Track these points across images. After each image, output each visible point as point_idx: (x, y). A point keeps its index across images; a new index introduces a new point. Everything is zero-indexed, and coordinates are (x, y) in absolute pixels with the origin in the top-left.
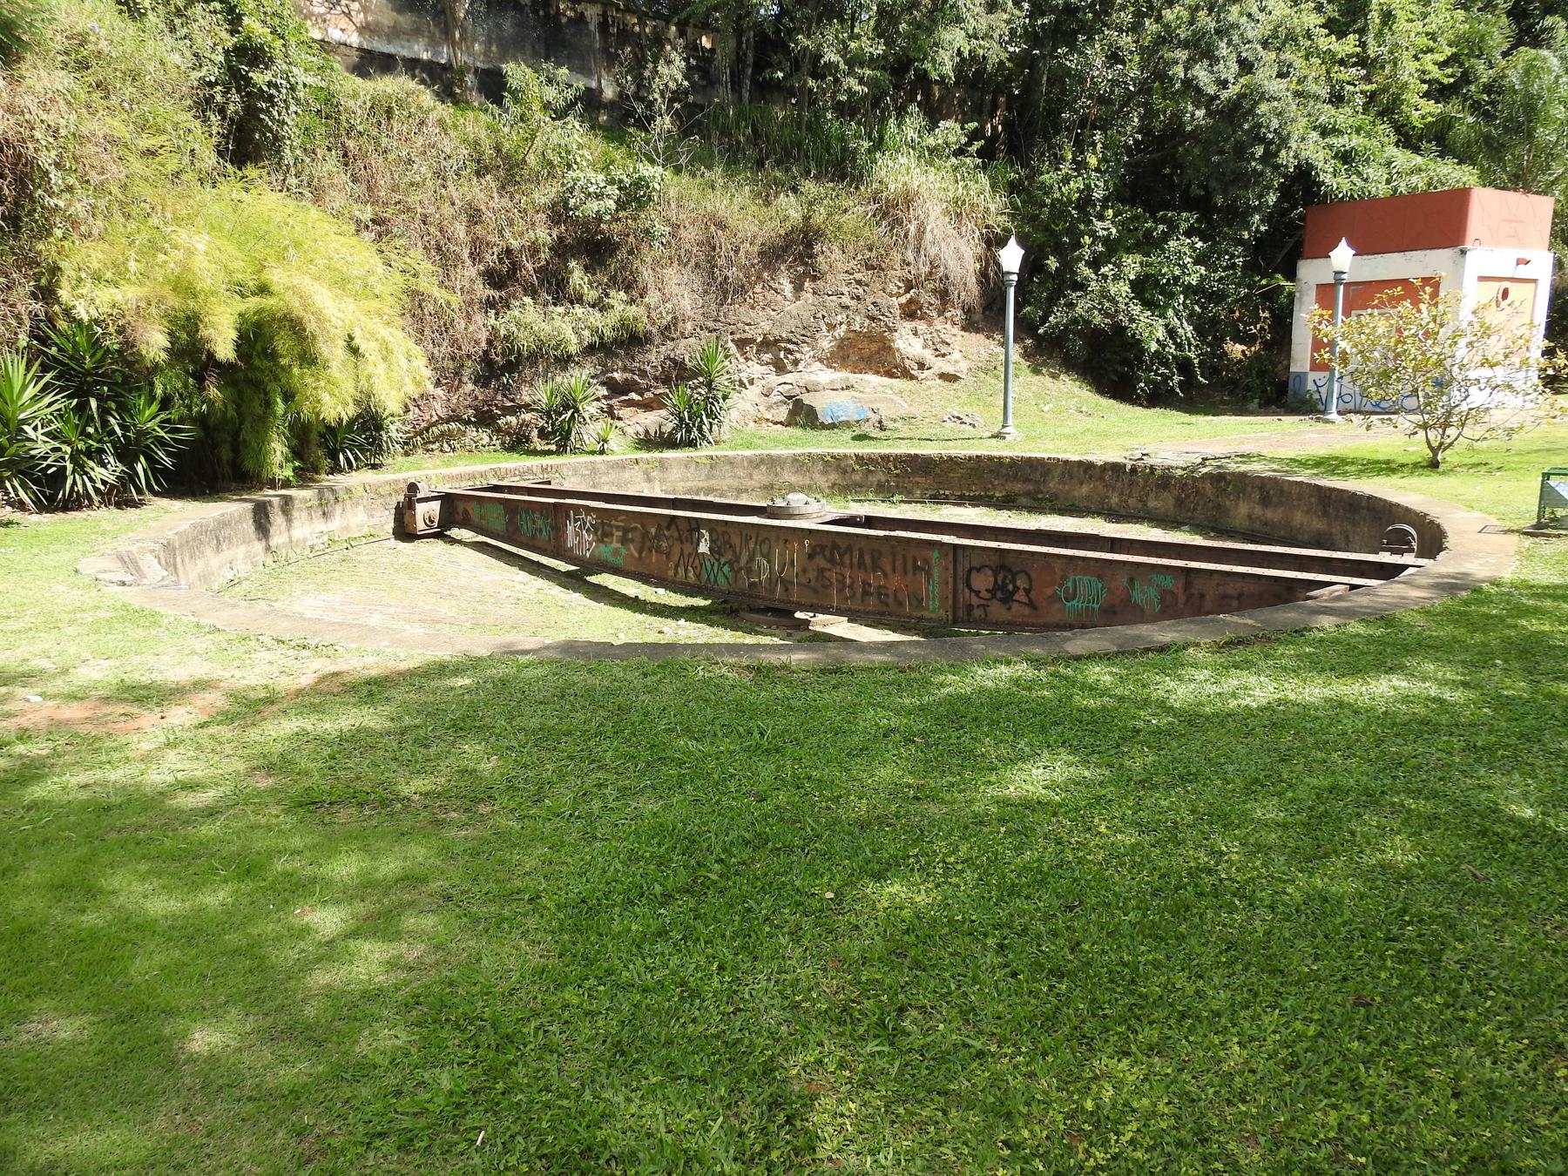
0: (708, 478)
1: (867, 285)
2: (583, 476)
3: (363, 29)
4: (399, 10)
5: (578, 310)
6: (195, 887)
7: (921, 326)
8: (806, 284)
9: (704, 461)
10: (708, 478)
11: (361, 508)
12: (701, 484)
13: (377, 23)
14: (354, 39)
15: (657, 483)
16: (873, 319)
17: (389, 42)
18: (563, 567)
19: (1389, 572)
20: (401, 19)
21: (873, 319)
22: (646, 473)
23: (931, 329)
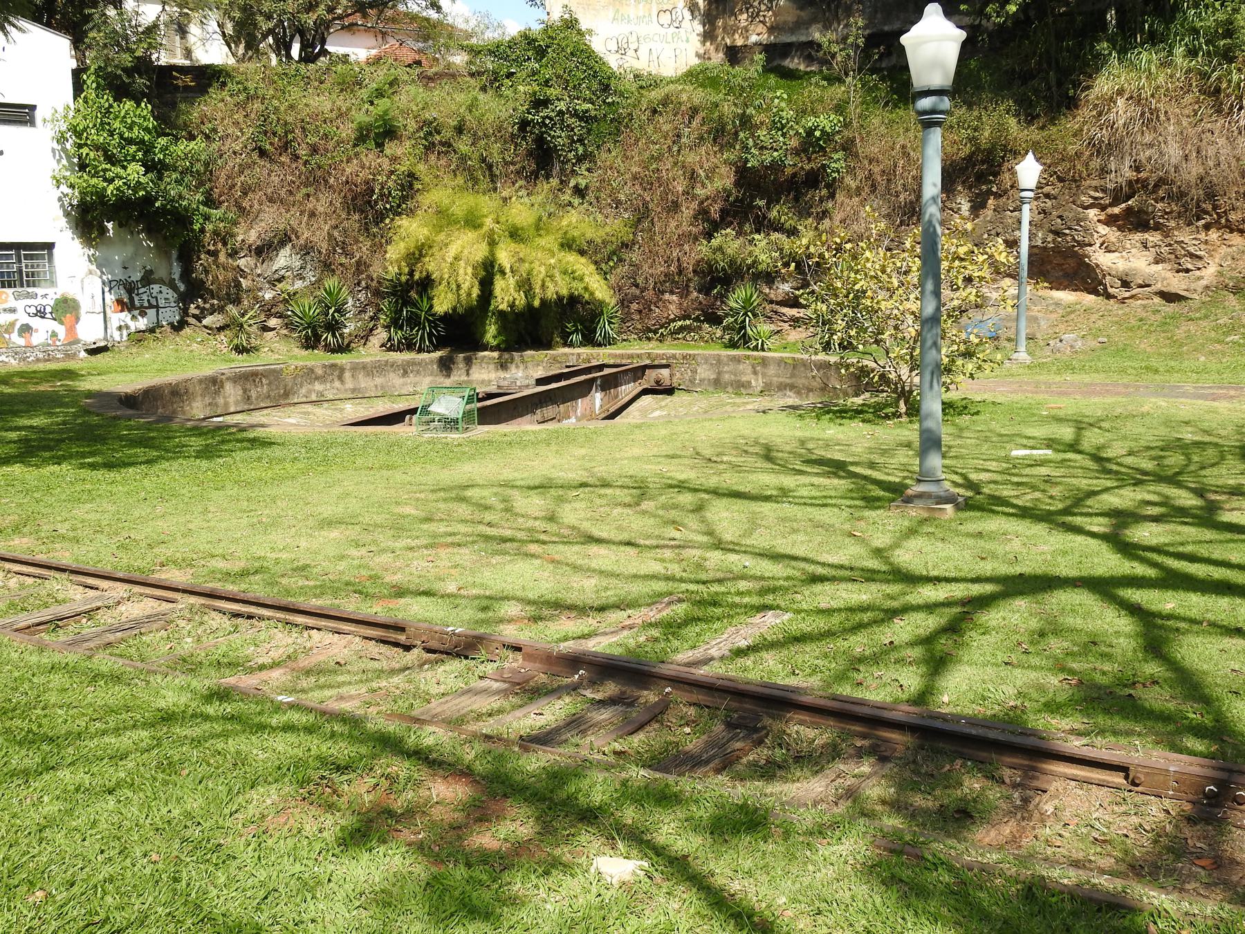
0: (792, 376)
1: (1055, 198)
2: (712, 364)
3: (771, 30)
4: (801, 8)
5: (775, 236)
6: (84, 422)
7: (1153, 237)
8: (990, 202)
9: (790, 361)
10: (792, 376)
11: (541, 368)
12: (788, 381)
13: (785, 22)
14: (764, 38)
15: (760, 376)
16: (1057, 233)
17: (793, 33)
18: (1012, 511)
19: (540, 382)
20: (803, 14)
21: (1057, 233)
22: (753, 367)
23: (1168, 240)
